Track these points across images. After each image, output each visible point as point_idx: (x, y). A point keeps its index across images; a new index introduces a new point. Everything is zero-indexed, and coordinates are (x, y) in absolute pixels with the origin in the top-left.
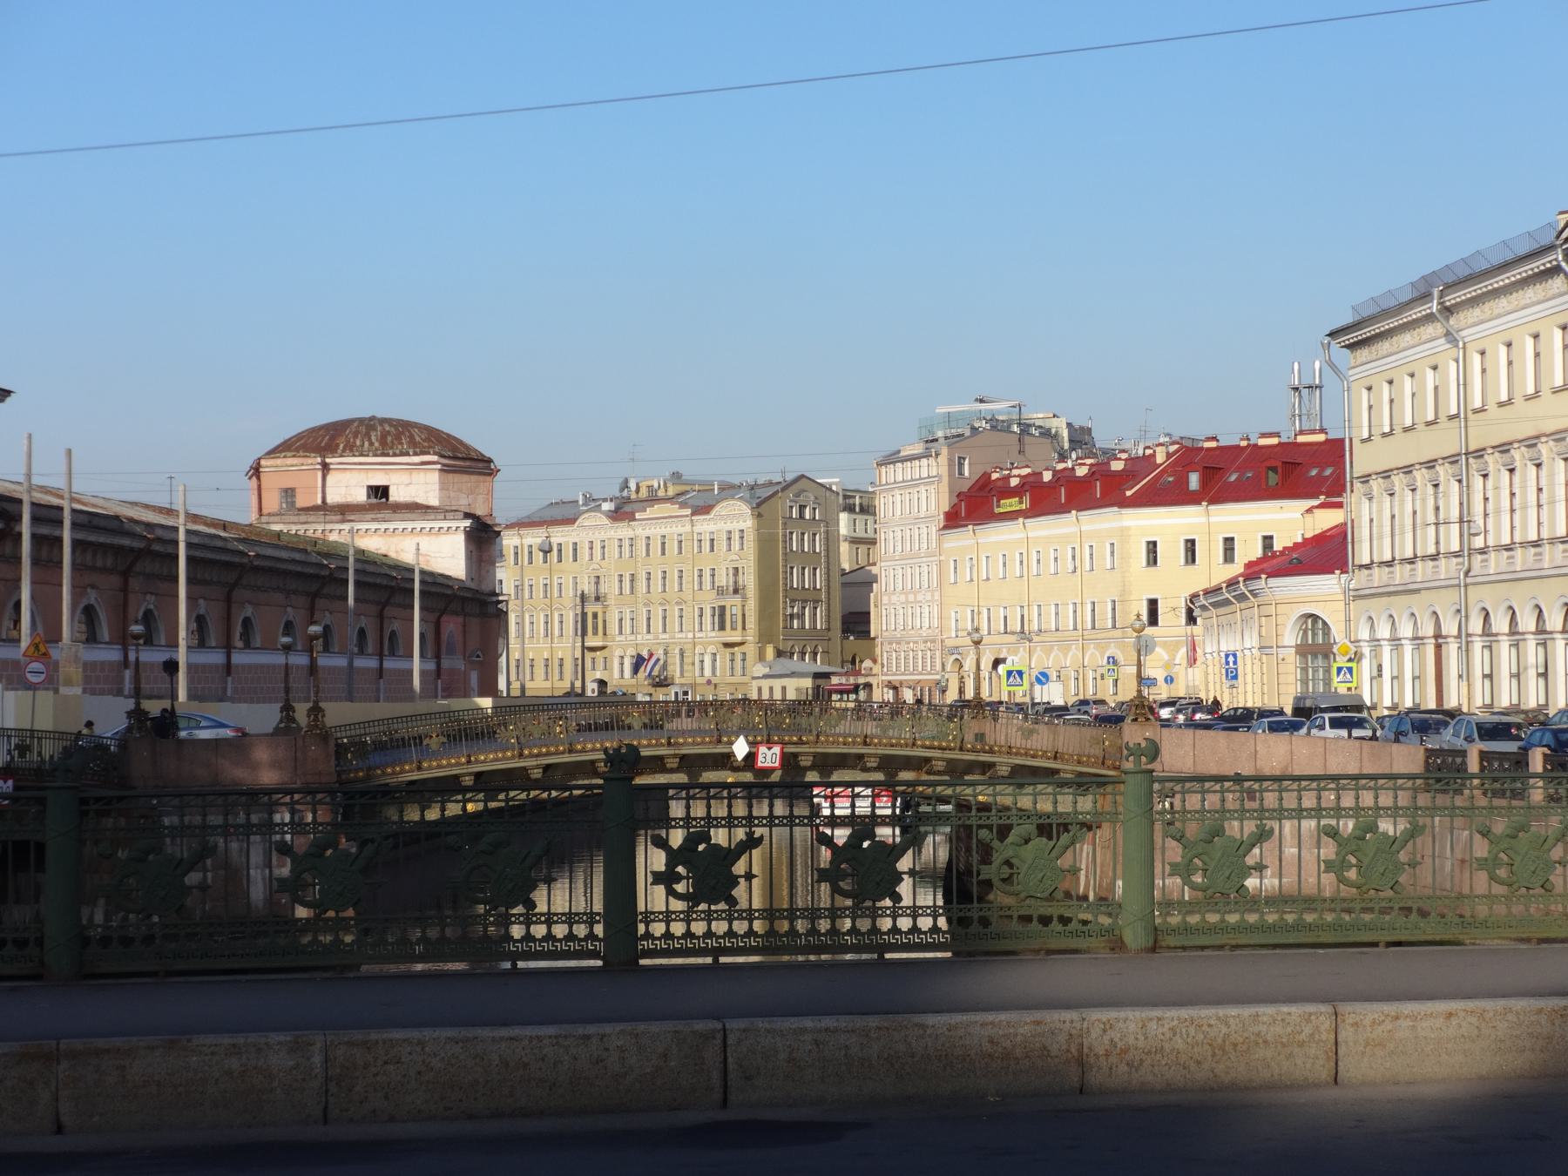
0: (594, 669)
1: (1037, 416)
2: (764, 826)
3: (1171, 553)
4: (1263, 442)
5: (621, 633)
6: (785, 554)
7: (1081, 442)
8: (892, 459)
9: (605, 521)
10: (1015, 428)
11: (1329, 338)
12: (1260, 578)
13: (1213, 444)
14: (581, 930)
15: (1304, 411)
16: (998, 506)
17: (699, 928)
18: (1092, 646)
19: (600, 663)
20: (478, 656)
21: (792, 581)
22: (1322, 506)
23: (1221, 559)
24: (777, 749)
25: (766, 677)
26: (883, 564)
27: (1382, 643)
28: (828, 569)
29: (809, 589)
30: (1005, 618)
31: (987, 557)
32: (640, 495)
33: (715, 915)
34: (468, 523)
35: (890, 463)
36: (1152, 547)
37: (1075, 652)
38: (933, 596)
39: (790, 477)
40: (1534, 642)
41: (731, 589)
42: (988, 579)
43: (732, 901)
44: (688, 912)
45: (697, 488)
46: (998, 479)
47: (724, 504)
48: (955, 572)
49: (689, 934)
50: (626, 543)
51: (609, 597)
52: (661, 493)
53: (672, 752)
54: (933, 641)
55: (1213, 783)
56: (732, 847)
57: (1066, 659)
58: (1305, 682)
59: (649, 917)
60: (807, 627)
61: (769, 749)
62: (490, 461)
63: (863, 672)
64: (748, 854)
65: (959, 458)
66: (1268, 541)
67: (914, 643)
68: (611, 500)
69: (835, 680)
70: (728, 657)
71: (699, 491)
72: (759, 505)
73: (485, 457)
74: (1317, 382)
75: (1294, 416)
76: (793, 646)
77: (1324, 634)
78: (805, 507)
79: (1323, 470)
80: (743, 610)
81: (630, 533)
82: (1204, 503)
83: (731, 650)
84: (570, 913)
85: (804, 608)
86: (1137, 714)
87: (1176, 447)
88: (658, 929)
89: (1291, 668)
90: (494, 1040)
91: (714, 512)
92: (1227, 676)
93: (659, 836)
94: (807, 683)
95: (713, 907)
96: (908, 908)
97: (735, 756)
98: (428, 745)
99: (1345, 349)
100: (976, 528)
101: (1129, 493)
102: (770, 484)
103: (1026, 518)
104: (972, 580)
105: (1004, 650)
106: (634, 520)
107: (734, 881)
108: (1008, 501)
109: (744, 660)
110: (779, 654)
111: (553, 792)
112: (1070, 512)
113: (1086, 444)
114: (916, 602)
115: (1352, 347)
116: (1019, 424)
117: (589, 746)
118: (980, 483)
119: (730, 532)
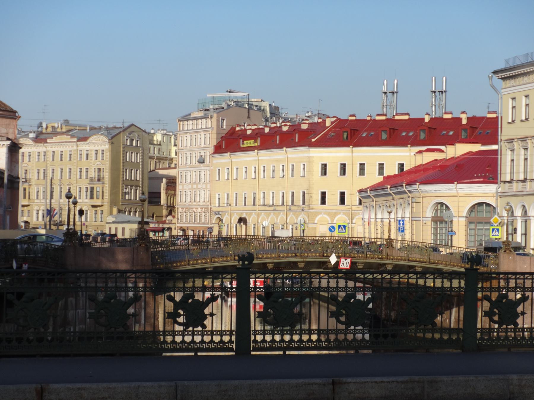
0: (23, 216)
1: (254, 100)
2: (529, 291)
3: (334, 170)
4: (378, 118)
5: (37, 198)
6: (124, 163)
7: (275, 114)
8: (186, 118)
9: (31, 142)
10: (246, 106)
11: (492, 74)
12: (416, 184)
13: (353, 118)
14: (226, 338)
15: (388, 104)
16: (243, 144)
17: (188, 339)
18: (291, 213)
19: (26, 213)
20: (10, 208)
21: (126, 176)
22: (427, 150)
23: (358, 174)
24: (349, 260)
25: (114, 222)
26: (179, 170)
27: (518, 218)
28: (143, 171)
29: (128, 180)
30: (245, 198)
31: (237, 168)
32: (48, 130)
33: (224, 333)
34: (9, 143)
35: (185, 121)
36: (324, 166)
37: (282, 215)
38: (206, 186)
39: (126, 125)
40: (521, 220)
41: (97, 179)
42: (237, 179)
43: (204, 327)
44: (345, 330)
45: (77, 128)
46: (239, 130)
47: (94, 137)
48: (219, 175)
49: (183, 342)
50: (42, 154)
51: (32, 180)
52: (59, 130)
53: (302, 260)
54: (206, 208)
55: (377, 277)
56: (205, 300)
57: (277, 219)
58: (435, 235)
59: (255, 333)
60: (132, 199)
61: (346, 260)
62: (16, 112)
63: (167, 222)
64: (211, 303)
65: (222, 119)
66: (401, 166)
67: (196, 208)
68: (34, 133)
69: (152, 225)
70: (94, 212)
71: (79, 130)
72: (112, 138)
73: (13, 110)
74: (395, 90)
75: (384, 106)
76: (126, 208)
77: (440, 212)
78: (133, 140)
79: (408, 133)
80: (103, 190)
81: (44, 149)
82: (351, 147)
83: (96, 209)
84: (222, 330)
85: (131, 189)
86: (506, 249)
87: (335, 119)
88: (259, 338)
89: (429, 228)
90: (389, 382)
91: (88, 141)
92: (399, 230)
93: (170, 295)
94: (136, 226)
95: (356, 328)
96: (209, 331)
97: (331, 263)
98: (193, 253)
99: (500, 80)
100: (231, 154)
101: (313, 140)
102: (115, 128)
103: (259, 150)
104: (228, 179)
105: (244, 214)
106: (47, 143)
107: (205, 317)
108: (248, 141)
109: (102, 214)
110: (119, 211)
111: (233, 275)
112: (283, 148)
113: (277, 115)
114: (197, 188)
115: (504, 79)
116: (248, 104)
117: (265, 256)
118: (230, 133)
119: (97, 151)
